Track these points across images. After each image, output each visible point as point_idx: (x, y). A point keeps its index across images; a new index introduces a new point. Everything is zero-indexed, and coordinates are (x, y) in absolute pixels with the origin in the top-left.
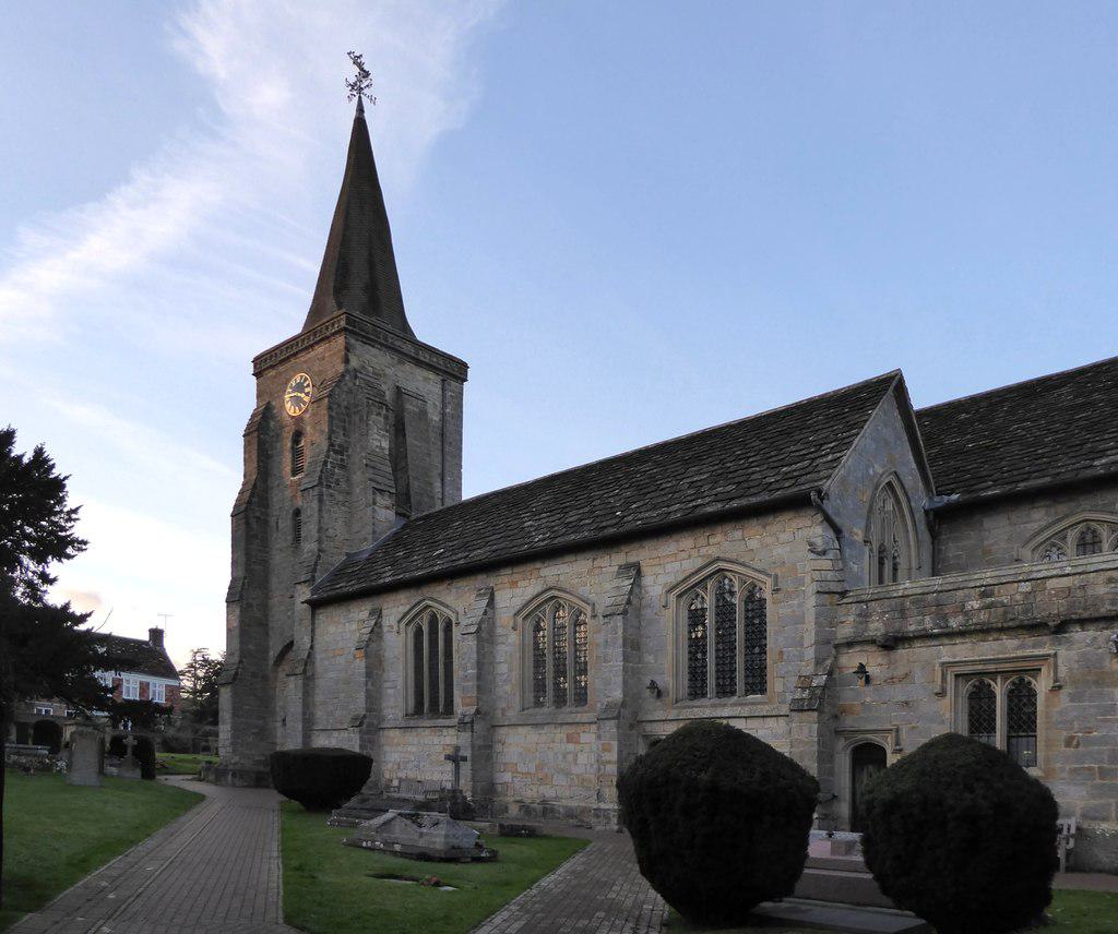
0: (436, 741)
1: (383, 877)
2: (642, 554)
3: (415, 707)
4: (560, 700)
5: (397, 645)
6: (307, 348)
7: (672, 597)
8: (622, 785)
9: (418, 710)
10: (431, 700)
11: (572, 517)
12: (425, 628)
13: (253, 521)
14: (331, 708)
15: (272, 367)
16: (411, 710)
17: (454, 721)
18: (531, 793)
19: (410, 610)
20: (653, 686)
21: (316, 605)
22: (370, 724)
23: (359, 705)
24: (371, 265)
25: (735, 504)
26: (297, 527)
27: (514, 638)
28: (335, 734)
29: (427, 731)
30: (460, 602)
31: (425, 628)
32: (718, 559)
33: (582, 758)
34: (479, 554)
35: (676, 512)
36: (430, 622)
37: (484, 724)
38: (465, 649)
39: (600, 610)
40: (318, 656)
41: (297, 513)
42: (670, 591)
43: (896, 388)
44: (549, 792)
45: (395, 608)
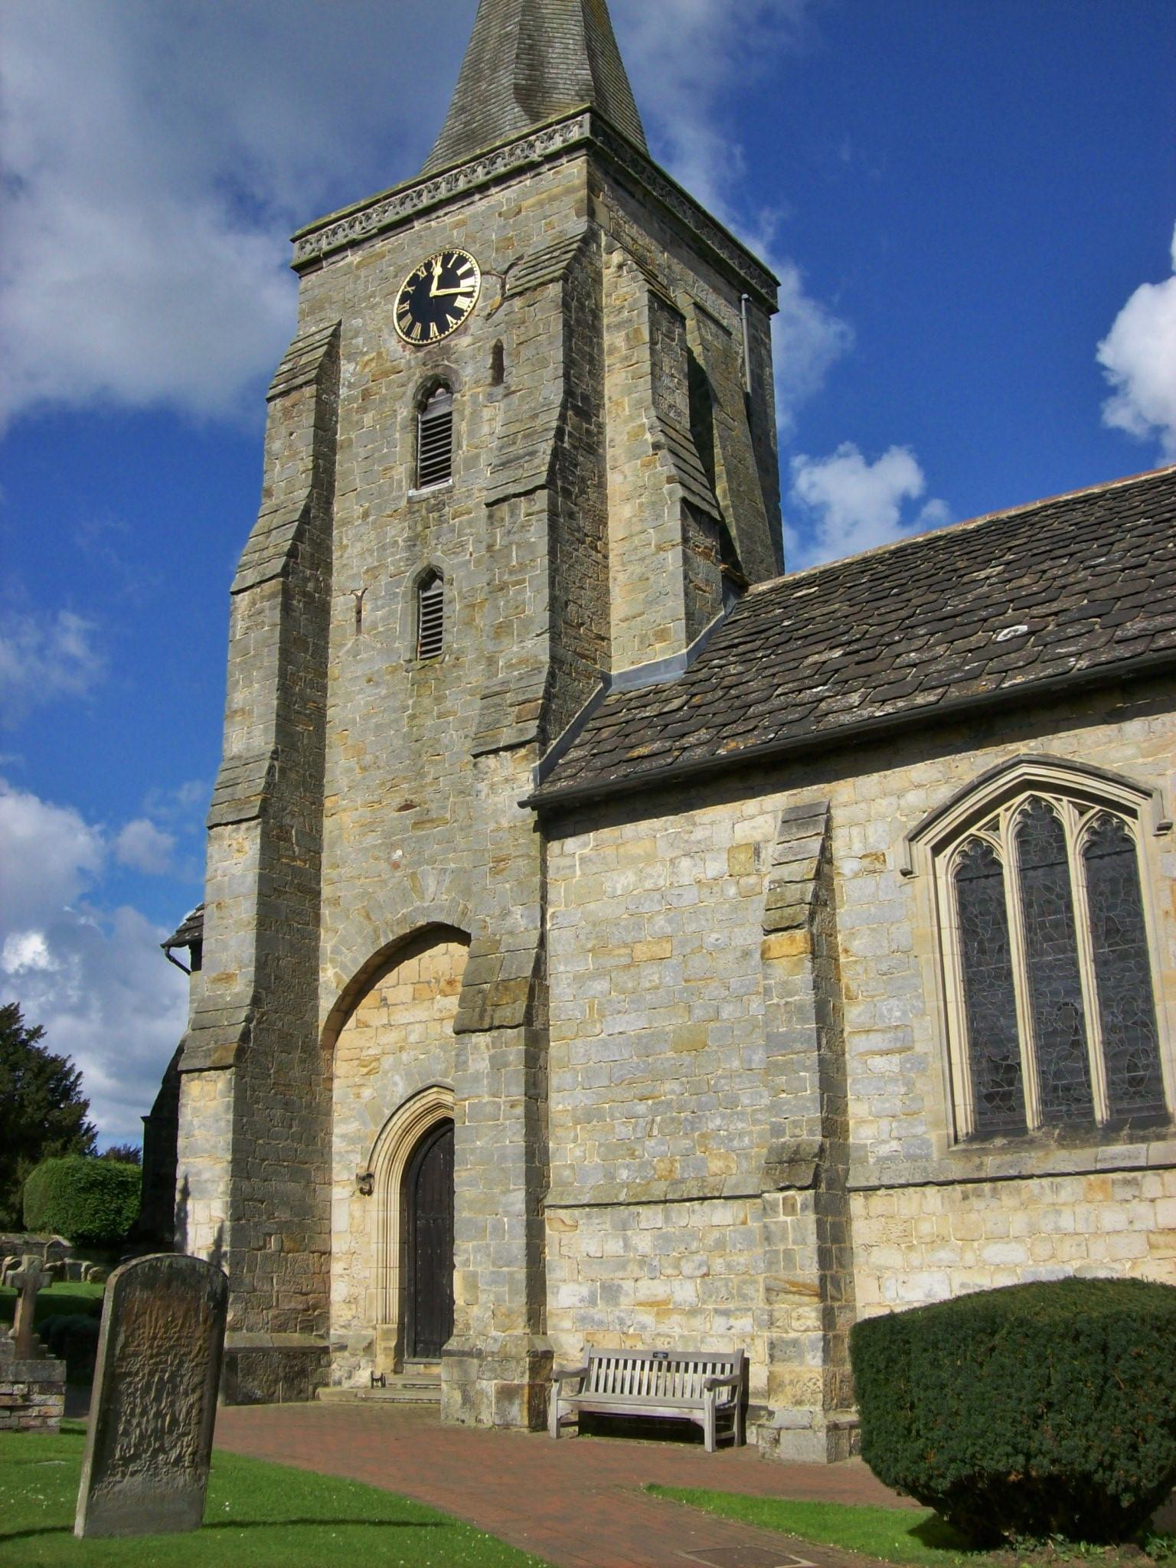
0: (1112, 1217)
1: (54, 1530)
3: (979, 1112)
6: (467, 194)
7: (922, 848)
12: (1007, 854)
13: (297, 603)
14: (624, 1131)
15: (353, 244)
16: (965, 1124)
19: (958, 799)
21: (558, 816)
28: (652, 1217)
29: (1070, 1188)
31: (1007, 854)
36: (1023, 837)
41: (429, 577)
42: (913, 838)
43: (696, 633)
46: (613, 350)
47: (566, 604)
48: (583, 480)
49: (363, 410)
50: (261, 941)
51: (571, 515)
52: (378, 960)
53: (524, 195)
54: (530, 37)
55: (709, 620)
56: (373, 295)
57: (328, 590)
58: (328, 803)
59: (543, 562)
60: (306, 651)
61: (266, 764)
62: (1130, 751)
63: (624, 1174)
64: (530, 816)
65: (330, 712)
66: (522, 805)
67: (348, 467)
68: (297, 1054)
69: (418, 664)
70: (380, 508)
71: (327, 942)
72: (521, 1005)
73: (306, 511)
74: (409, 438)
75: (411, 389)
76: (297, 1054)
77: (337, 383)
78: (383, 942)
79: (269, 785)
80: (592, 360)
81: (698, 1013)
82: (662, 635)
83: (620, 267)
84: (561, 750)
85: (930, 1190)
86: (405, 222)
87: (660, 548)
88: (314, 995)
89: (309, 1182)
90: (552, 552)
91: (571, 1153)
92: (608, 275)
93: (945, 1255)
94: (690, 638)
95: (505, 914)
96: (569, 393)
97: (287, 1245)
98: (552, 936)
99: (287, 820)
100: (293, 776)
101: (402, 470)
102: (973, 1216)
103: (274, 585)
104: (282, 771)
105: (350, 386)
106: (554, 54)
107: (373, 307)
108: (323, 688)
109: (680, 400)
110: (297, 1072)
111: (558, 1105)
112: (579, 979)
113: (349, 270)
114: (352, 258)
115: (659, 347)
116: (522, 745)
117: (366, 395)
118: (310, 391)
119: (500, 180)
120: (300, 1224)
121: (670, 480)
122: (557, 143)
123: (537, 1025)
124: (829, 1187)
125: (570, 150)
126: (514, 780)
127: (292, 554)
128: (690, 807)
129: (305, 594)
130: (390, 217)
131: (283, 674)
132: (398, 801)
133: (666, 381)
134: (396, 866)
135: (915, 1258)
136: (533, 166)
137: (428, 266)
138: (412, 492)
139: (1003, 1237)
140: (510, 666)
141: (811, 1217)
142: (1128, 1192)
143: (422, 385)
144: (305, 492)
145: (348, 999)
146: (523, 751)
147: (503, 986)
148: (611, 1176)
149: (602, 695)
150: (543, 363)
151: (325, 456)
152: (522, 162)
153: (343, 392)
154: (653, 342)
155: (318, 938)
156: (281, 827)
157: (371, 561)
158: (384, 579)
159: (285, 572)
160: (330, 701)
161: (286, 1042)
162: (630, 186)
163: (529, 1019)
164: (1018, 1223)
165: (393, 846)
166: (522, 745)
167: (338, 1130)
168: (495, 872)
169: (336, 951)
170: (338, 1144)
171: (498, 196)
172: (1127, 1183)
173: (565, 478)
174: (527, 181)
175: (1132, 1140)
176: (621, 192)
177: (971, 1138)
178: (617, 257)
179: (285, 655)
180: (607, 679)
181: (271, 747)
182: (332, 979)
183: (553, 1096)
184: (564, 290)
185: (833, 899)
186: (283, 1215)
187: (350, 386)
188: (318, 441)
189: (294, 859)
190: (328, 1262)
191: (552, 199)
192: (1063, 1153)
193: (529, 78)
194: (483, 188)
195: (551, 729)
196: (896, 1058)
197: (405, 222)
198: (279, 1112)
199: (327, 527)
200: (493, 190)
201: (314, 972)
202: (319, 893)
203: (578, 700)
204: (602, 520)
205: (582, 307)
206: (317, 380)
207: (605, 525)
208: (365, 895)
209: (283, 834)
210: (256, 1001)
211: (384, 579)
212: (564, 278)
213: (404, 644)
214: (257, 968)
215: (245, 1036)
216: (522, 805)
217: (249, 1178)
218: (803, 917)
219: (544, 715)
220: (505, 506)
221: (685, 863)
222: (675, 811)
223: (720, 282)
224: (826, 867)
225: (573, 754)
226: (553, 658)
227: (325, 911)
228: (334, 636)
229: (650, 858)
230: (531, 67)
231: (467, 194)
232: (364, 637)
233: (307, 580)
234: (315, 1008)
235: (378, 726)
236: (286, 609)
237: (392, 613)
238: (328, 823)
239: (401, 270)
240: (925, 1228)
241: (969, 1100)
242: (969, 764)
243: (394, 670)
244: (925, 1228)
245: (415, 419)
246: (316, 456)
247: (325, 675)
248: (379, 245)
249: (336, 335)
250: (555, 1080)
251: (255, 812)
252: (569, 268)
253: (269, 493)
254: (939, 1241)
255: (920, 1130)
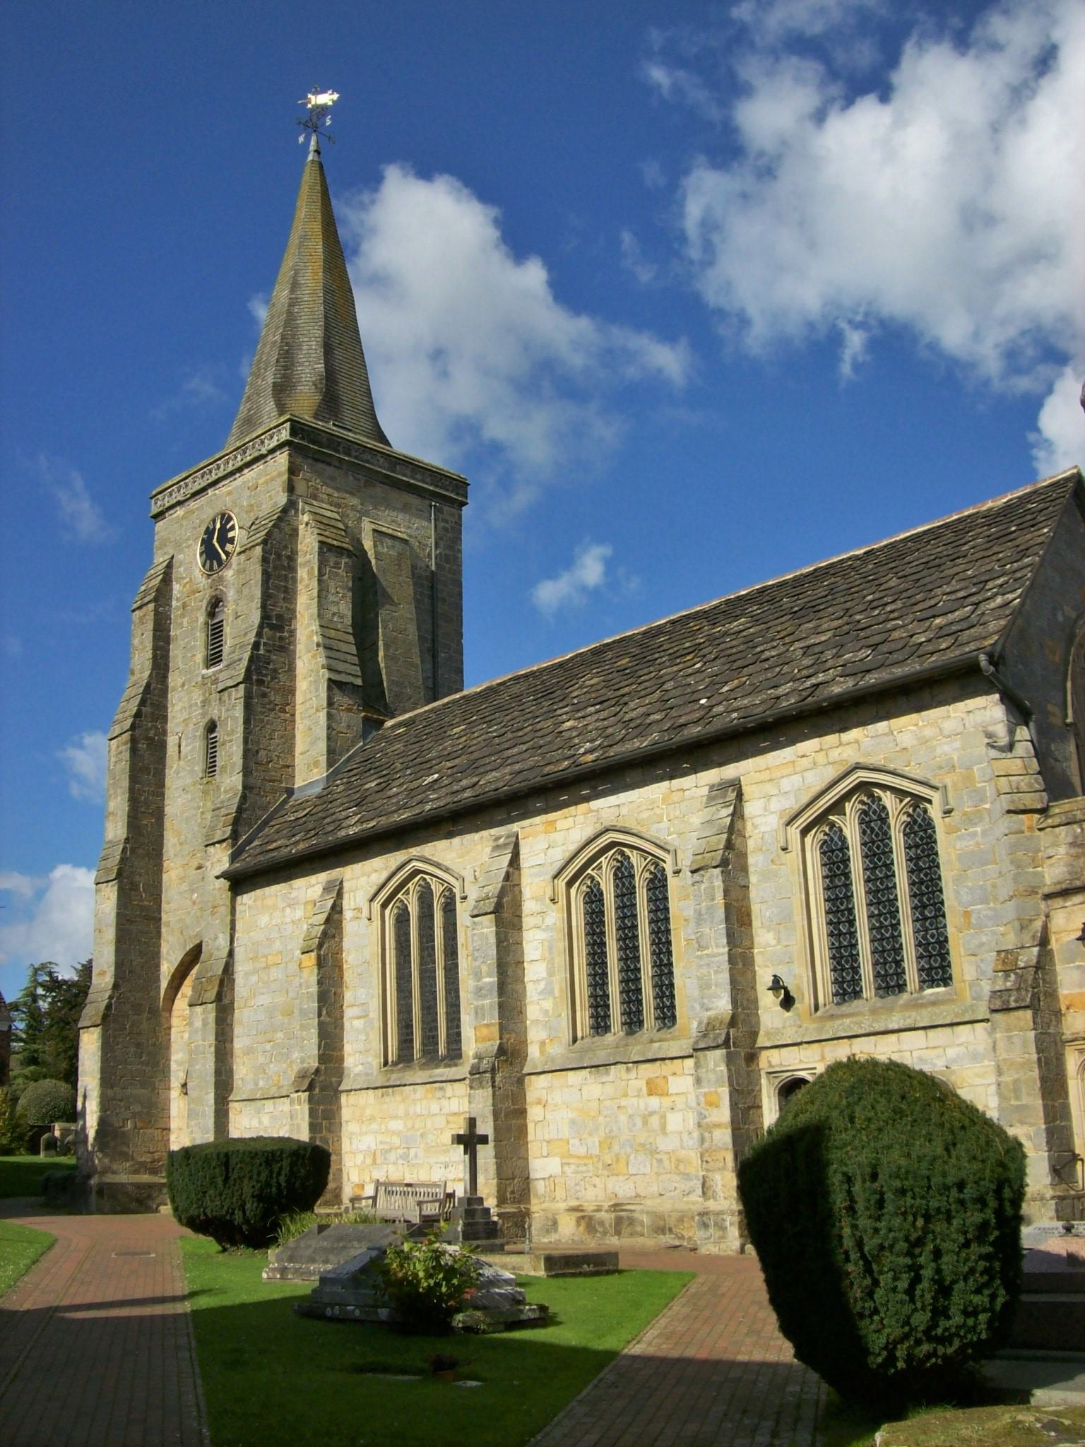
2: (747, 770)
4: (633, 1021)
5: (364, 942)
8: (747, 1189)
9: (405, 1056)
10: (422, 1039)
11: (634, 710)
13: (142, 746)
14: (261, 1060)
15: (180, 503)
17: (463, 1070)
18: (595, 1195)
20: (777, 985)
21: (240, 882)
22: (323, 1086)
23: (307, 1053)
24: (328, 349)
25: (872, 679)
26: (211, 748)
27: (555, 916)
30: (467, 859)
31: (413, 909)
32: (858, 767)
33: (675, 1121)
34: (496, 779)
35: (788, 696)
37: (507, 1066)
38: (476, 937)
39: (686, 862)
40: (240, 969)
41: (212, 727)
42: (371, 900)
43: (335, 761)
44: (623, 1189)
45: (363, 878)
46: (302, 579)
47: (257, 752)
48: (275, 670)
49: (183, 616)
50: (118, 951)
51: (264, 695)
52: (189, 958)
53: (259, 475)
54: (287, 344)
55: (348, 750)
56: (188, 539)
57: (165, 733)
58: (165, 864)
59: (241, 729)
60: (149, 774)
61: (121, 847)
62: (454, 855)
63: (261, 1083)
64: (224, 883)
65: (166, 809)
66: (217, 877)
67: (176, 652)
68: (145, 1015)
69: (205, 780)
70: (189, 680)
71: (164, 949)
72: (214, 992)
73: (148, 686)
74: (204, 635)
75: (205, 603)
76: (145, 1015)
77: (171, 598)
78: (188, 948)
79: (123, 860)
80: (286, 590)
81: (291, 994)
82: (316, 764)
83: (307, 524)
84: (249, 841)
85: (370, 1092)
86: (204, 490)
87: (318, 710)
88: (158, 980)
89: (154, 1089)
90: (247, 722)
91: (242, 1070)
92: (301, 527)
93: (374, 1126)
94: (330, 765)
95: (216, 938)
96: (265, 617)
97: (139, 1125)
98: (237, 950)
99: (137, 878)
100: (140, 851)
101: (200, 657)
102: (385, 1106)
103: (127, 736)
104: (133, 850)
105: (178, 599)
106: (301, 356)
107: (189, 547)
108: (163, 795)
109: (345, 608)
110: (145, 1026)
111: (239, 1043)
112: (247, 974)
113: (179, 519)
114: (180, 512)
115: (326, 577)
116: (224, 841)
117: (184, 606)
118: (151, 606)
119: (248, 465)
120: (148, 1113)
121: (323, 667)
122: (274, 443)
123: (226, 1001)
124: (322, 1090)
125: (280, 446)
126: (220, 859)
127: (138, 715)
128: (291, 879)
129: (148, 738)
130: (197, 487)
131: (132, 790)
132: (195, 864)
133: (331, 598)
134: (194, 903)
135: (364, 1128)
136: (262, 457)
137: (214, 521)
138: (204, 671)
139: (396, 1117)
140: (225, 791)
141: (306, 1107)
142: (439, 1094)
143: (209, 602)
144: (147, 673)
145: (176, 982)
146: (224, 844)
147: (210, 979)
148: (256, 1084)
149: (285, 802)
150: (251, 599)
151: (161, 648)
152: (256, 454)
153: (174, 603)
154: (321, 574)
155: (159, 946)
156: (132, 883)
157: (185, 715)
158: (191, 727)
159: (133, 727)
160: (167, 802)
161: (137, 1008)
162: (328, 460)
163: (219, 998)
164: (401, 1110)
165: (193, 891)
166: (224, 841)
167: (173, 1058)
168: (213, 914)
169: (168, 953)
170: (173, 1066)
171: (248, 474)
172: (441, 1089)
173: (259, 674)
174: (259, 467)
175: (446, 1066)
176: (320, 465)
177: (395, 1064)
178: (306, 518)
179: (133, 779)
180: (290, 792)
181: (125, 836)
182: (167, 969)
183: (236, 1041)
184: (263, 550)
185: (341, 933)
186: (137, 1108)
187: (178, 599)
188: (156, 638)
189: (142, 900)
190: (168, 1135)
191: (272, 479)
192: (420, 1073)
193: (284, 376)
194: (240, 469)
195: (241, 829)
196: (362, 1021)
197: (204, 490)
198: (132, 1049)
199: (164, 692)
200: (246, 471)
201: (158, 966)
202: (160, 919)
203: (265, 809)
204: (292, 691)
205: (279, 556)
206: (155, 600)
207: (294, 695)
208: (181, 920)
209: (134, 887)
210: (116, 986)
211: (191, 727)
212: (265, 542)
213: (199, 768)
214: (116, 968)
215: (109, 1007)
216: (217, 877)
217: (112, 1088)
218: (314, 946)
219: (236, 823)
220: (226, 693)
221: (288, 910)
222: (285, 881)
223: (414, 500)
224: (738, 825)
225: (256, 843)
226: (245, 787)
227: (164, 930)
228: (168, 761)
229: (275, 907)
230: (286, 368)
231: (232, 473)
232: (182, 763)
233: (148, 730)
234: (159, 987)
235: (187, 818)
236: (134, 751)
237: (194, 748)
238: (165, 877)
239: (202, 521)
240: (368, 1112)
241: (396, 1043)
242: (393, 859)
243: (194, 783)
244: (368, 1112)
245: (207, 624)
246: (155, 649)
247: (163, 786)
248: (193, 505)
249: (170, 566)
250: (238, 1030)
251: (114, 876)
252: (269, 534)
253: (133, 673)
254: (372, 1119)
255: (370, 1059)
